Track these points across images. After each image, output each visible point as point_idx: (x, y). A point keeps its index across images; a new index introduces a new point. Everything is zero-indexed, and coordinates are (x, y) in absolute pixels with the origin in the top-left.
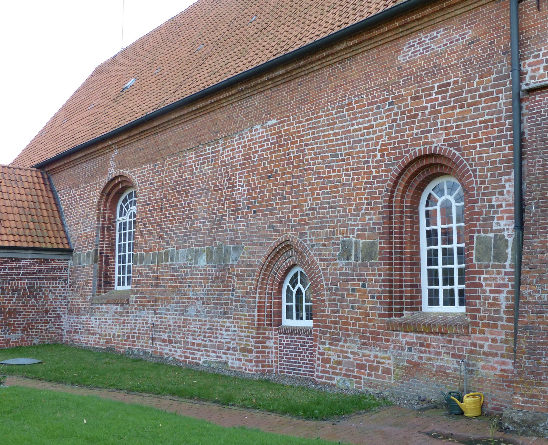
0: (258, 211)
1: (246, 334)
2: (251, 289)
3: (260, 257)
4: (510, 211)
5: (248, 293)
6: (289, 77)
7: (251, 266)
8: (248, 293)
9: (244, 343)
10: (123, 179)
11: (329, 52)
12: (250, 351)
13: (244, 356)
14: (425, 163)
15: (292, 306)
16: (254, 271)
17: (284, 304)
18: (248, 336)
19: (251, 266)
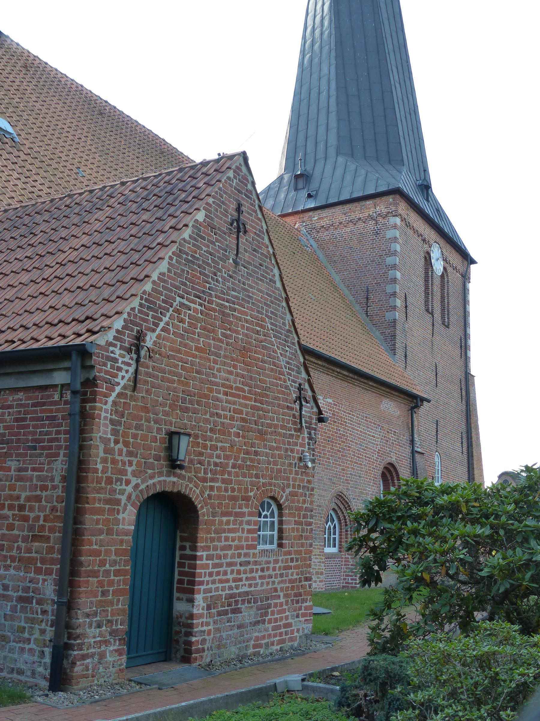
0: (322, 464)
1: (319, 560)
2: (320, 524)
3: (325, 500)
4: (186, 489)
5: (319, 527)
6: (345, 379)
7: (320, 506)
8: (319, 527)
9: (317, 567)
10: (272, 193)
11: (366, 381)
12: (322, 574)
13: (318, 578)
14: (392, 469)
15: (36, 476)
16: (322, 510)
17: (337, 536)
18: (320, 562)
19: (320, 506)
